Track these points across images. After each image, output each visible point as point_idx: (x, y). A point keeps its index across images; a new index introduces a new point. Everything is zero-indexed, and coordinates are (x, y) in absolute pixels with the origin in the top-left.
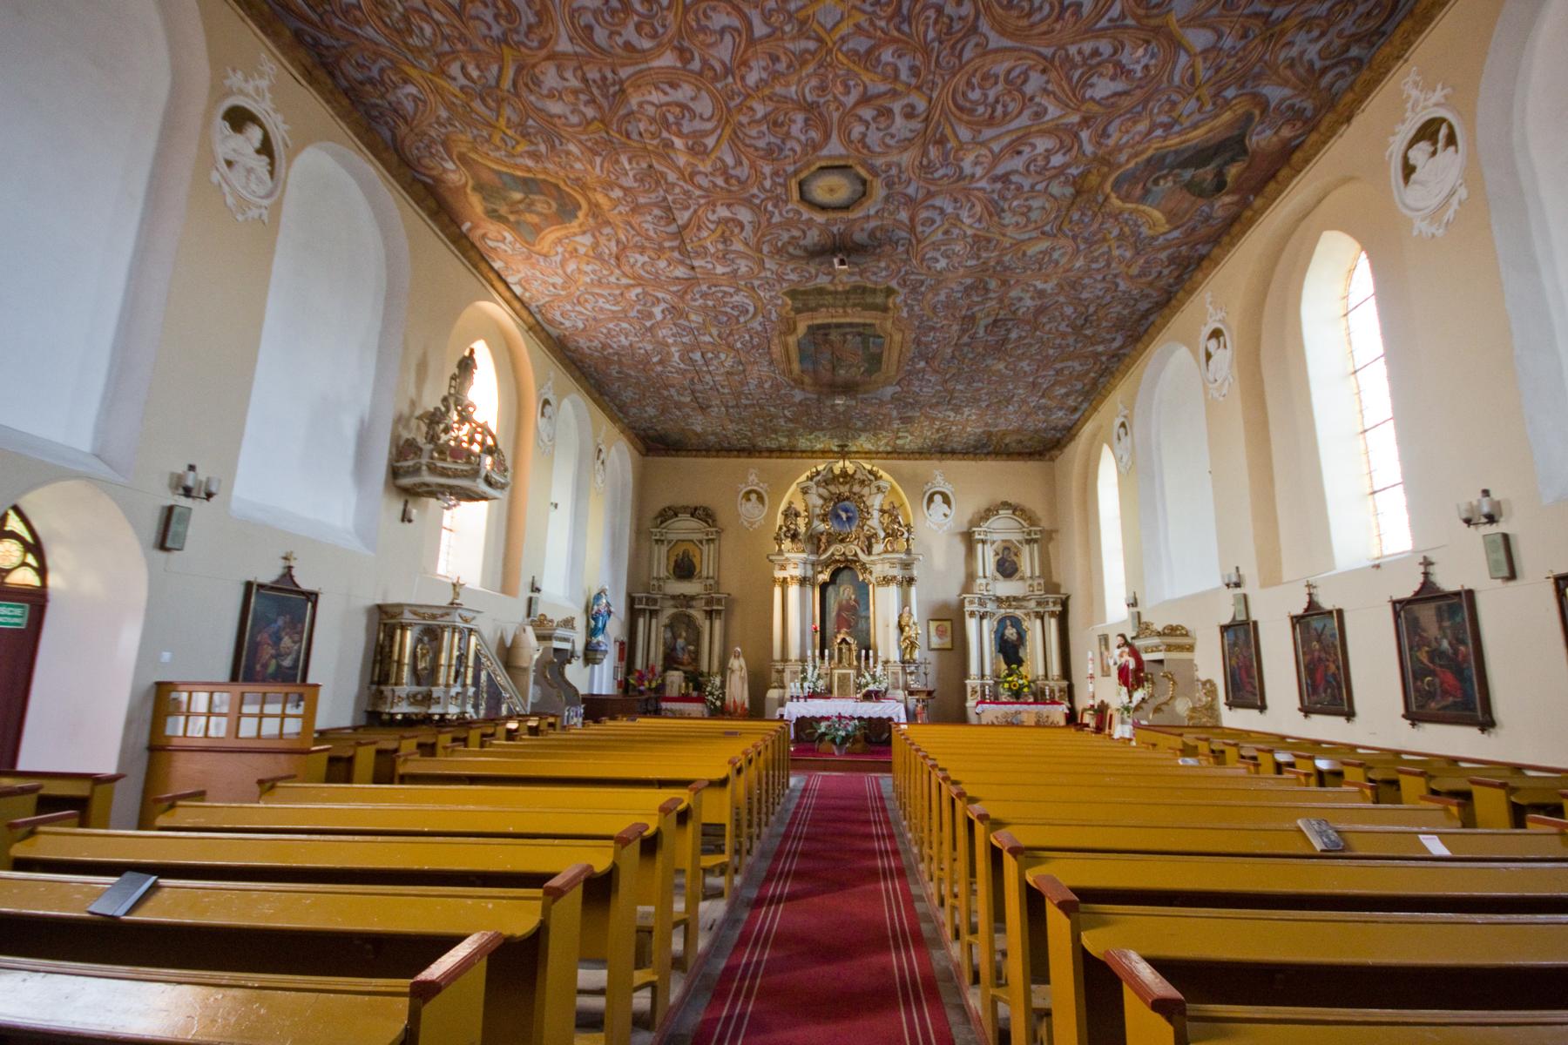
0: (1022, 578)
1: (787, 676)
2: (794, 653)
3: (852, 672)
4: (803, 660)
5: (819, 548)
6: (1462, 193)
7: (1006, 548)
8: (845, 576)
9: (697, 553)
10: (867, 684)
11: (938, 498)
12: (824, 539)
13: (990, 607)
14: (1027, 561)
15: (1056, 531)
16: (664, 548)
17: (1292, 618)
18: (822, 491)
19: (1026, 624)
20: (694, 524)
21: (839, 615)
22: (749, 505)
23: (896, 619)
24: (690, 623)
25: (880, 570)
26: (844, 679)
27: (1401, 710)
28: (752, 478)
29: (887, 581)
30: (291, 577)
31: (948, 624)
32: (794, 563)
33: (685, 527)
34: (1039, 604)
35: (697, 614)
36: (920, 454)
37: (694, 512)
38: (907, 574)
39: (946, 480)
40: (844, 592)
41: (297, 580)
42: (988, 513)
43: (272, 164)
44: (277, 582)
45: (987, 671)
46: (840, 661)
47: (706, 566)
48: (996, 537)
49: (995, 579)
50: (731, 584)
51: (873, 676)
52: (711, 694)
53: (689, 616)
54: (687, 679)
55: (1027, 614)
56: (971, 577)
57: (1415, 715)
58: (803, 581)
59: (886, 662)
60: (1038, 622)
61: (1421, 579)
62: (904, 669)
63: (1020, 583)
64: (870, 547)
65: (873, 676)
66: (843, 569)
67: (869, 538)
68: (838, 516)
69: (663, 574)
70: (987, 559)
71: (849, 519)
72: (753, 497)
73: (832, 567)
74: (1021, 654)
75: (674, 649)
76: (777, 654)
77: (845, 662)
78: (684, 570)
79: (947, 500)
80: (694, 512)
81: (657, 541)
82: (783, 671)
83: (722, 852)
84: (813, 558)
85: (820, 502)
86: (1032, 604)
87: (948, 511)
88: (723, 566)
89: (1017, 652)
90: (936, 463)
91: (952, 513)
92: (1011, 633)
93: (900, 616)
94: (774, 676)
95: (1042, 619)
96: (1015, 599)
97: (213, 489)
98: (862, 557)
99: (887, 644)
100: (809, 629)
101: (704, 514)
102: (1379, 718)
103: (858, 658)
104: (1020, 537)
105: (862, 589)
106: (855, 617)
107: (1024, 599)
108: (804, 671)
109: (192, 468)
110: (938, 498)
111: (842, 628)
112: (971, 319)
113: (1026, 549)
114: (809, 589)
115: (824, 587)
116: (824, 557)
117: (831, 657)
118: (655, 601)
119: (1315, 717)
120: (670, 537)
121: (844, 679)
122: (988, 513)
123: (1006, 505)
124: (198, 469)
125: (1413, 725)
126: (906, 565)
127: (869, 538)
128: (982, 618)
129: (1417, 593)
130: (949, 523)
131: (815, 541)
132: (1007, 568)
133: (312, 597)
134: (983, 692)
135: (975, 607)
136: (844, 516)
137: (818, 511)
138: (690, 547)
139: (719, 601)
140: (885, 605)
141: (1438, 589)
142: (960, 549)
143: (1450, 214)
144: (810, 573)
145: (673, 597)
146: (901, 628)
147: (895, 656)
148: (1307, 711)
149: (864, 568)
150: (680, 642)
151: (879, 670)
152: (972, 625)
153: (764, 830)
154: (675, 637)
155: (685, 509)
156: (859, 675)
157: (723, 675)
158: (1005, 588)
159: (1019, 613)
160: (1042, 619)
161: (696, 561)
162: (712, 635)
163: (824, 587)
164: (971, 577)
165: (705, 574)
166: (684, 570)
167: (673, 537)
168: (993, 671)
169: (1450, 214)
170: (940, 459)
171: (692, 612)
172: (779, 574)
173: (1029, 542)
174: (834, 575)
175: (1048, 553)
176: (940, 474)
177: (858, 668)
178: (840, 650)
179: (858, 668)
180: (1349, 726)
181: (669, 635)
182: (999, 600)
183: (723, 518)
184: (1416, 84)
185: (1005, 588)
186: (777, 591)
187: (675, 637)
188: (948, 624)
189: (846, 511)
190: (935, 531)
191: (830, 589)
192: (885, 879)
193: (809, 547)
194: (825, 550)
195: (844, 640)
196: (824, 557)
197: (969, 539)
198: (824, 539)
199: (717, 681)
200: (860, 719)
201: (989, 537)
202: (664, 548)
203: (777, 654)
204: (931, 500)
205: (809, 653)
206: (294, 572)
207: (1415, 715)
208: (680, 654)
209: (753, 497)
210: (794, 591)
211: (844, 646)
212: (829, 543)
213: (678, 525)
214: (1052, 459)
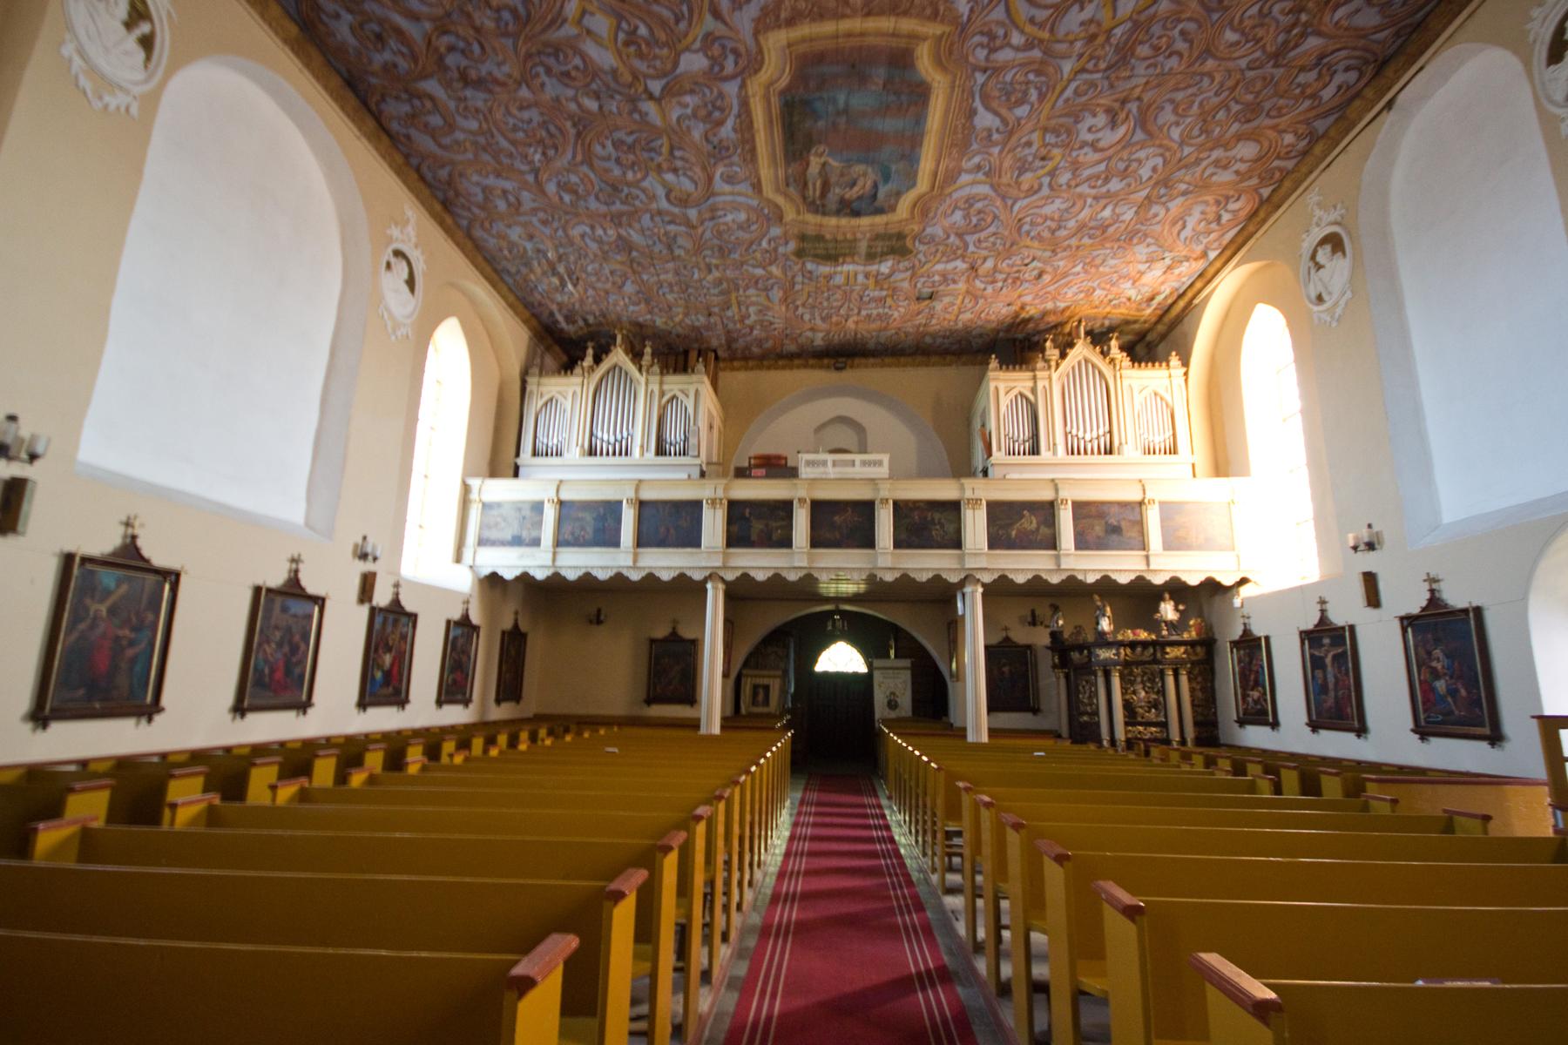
6: (1349, 294)
17: (1402, 619)
27: (1410, 724)
30: (137, 550)
41: (146, 553)
43: (148, 58)
44: (114, 554)
57: (1423, 731)
61: (1428, 595)
83: (615, 543)
97: (39, 449)
102: (1390, 733)
109: (12, 418)
112: (1096, 198)
119: (1323, 733)
124: (21, 421)
125: (1422, 739)
129: (1424, 609)
133: (173, 577)
141: (1446, 606)
143: (1339, 311)
148: (1315, 726)
153: (736, 919)
169: (1339, 311)
180: (1361, 742)
184: (1319, 204)
192: (923, 989)
206: (140, 543)
207: (1423, 731)
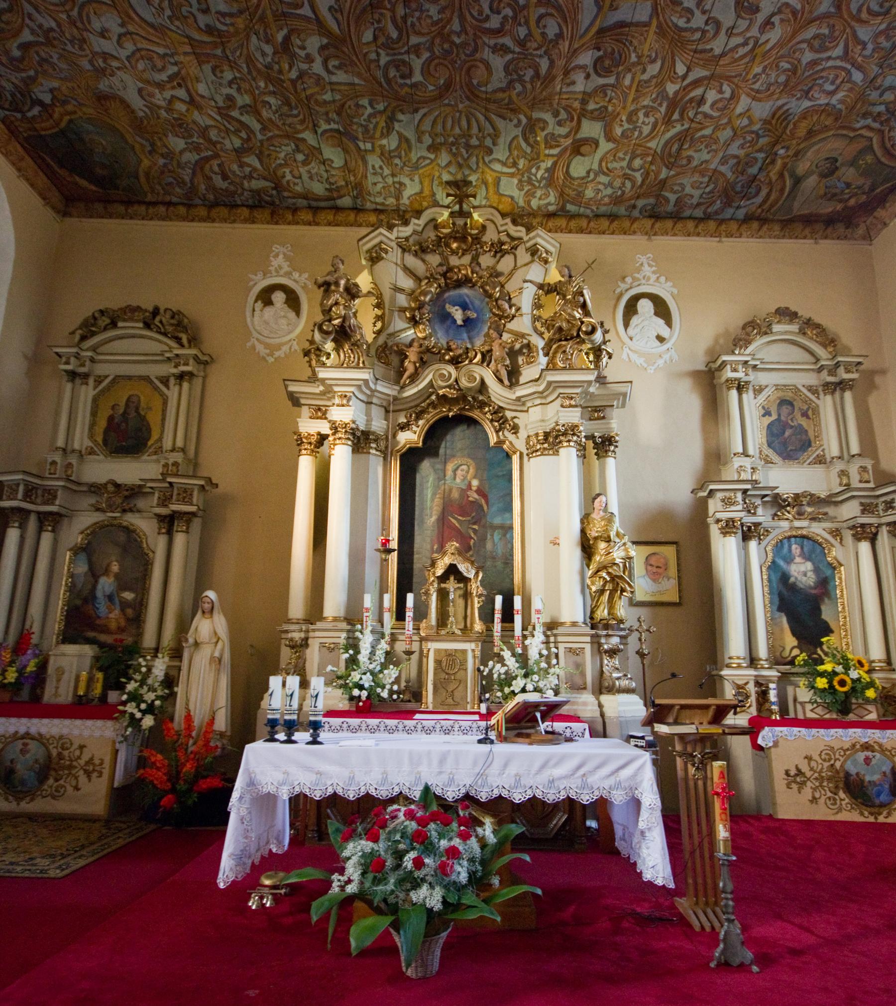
0: (821, 460)
1: (313, 655)
2: (335, 601)
3: (471, 648)
4: (352, 617)
5: (400, 372)
7: (783, 402)
8: (459, 437)
9: (157, 403)
10: (509, 679)
11: (645, 306)
12: (412, 355)
13: (763, 516)
14: (834, 424)
15: (883, 372)
16: (87, 393)
18: (411, 261)
19: (836, 553)
20: (152, 344)
21: (442, 520)
22: (269, 312)
23: (577, 526)
24: (133, 548)
25: (535, 420)
26: (449, 665)
28: (278, 262)
29: (552, 440)
31: (669, 552)
32: (347, 393)
33: (134, 353)
34: (867, 509)
35: (144, 524)
36: (612, 217)
37: (151, 319)
38: (597, 429)
39: (659, 273)
40: (453, 474)
42: (754, 328)
45: (762, 651)
46: (442, 620)
47: (172, 433)
48: (763, 378)
49: (768, 462)
50: (223, 465)
51: (523, 659)
52: (135, 697)
53: (129, 531)
54: (98, 663)
55: (836, 533)
56: (715, 457)
58: (361, 441)
59: (551, 626)
60: (864, 547)
62: (596, 642)
63: (819, 469)
64: (513, 375)
65: (523, 659)
66: (455, 418)
67: (513, 354)
68: (446, 317)
69: (81, 441)
70: (747, 423)
71: (467, 321)
72: (279, 297)
73: (432, 416)
74: (826, 614)
75: (91, 598)
76: (297, 607)
77: (454, 624)
78: (127, 435)
79: (662, 310)
80: (151, 319)
81: (73, 375)
82: (305, 643)
84: (385, 389)
85: (407, 283)
86: (850, 511)
87: (665, 332)
88: (208, 426)
89: (816, 611)
90: (639, 240)
91: (674, 335)
92: (802, 571)
93: (585, 519)
94: (286, 654)
95: (873, 540)
96: (815, 500)
98: (498, 392)
99: (554, 583)
100: (373, 541)
101: (178, 327)
103: (487, 616)
104: (812, 379)
105: (497, 466)
106: (481, 521)
107: (830, 501)
108: (353, 645)
110: (645, 306)
111: (453, 553)
113: (826, 405)
114: (375, 462)
115: (411, 460)
116: (411, 391)
117: (421, 614)
118: (50, 495)
120: (100, 369)
121: (449, 665)
122: (754, 328)
123: (786, 314)
126: (596, 411)
127: (513, 354)
128: (746, 538)
130: (668, 353)
131: (389, 356)
132: (790, 438)
134: (763, 695)
135: (736, 513)
136: (458, 315)
137: (402, 300)
138: (144, 394)
139: (186, 495)
140: (548, 498)
142: (692, 404)
144: (378, 425)
145: (95, 489)
146: (587, 549)
147: (572, 609)
149: (500, 418)
150: (106, 584)
151: (535, 645)
152: (726, 552)
154: (94, 574)
155: (130, 312)
156: (488, 654)
157: (177, 654)
158: (788, 479)
159: (818, 530)
160: (873, 540)
161: (153, 419)
162: (172, 559)
163: (411, 460)
164: (715, 457)
165: (167, 444)
166: (127, 435)
167: (109, 370)
168: (771, 649)
170: (650, 233)
171: (132, 519)
172: (310, 426)
173: (832, 388)
174: (435, 435)
175: (867, 410)
176: (648, 261)
177: (486, 639)
178: (443, 595)
179: (486, 639)
181: (82, 568)
182: (778, 503)
183: (215, 338)
185: (788, 479)
186: (306, 467)
187: (94, 574)
188: (669, 552)
189: (464, 307)
190: (647, 362)
191: (426, 467)
193: (380, 369)
194: (414, 378)
195: (452, 570)
196: (411, 391)
197: (710, 384)
198: (412, 355)
199: (160, 667)
200: (498, 807)
201: (752, 377)
202: (87, 393)
203: (297, 607)
204: (631, 309)
205: (368, 601)
208: (102, 607)
209: (279, 297)
210: (341, 456)
211: (451, 585)
212: (423, 363)
213: (117, 346)
214: (868, 237)
